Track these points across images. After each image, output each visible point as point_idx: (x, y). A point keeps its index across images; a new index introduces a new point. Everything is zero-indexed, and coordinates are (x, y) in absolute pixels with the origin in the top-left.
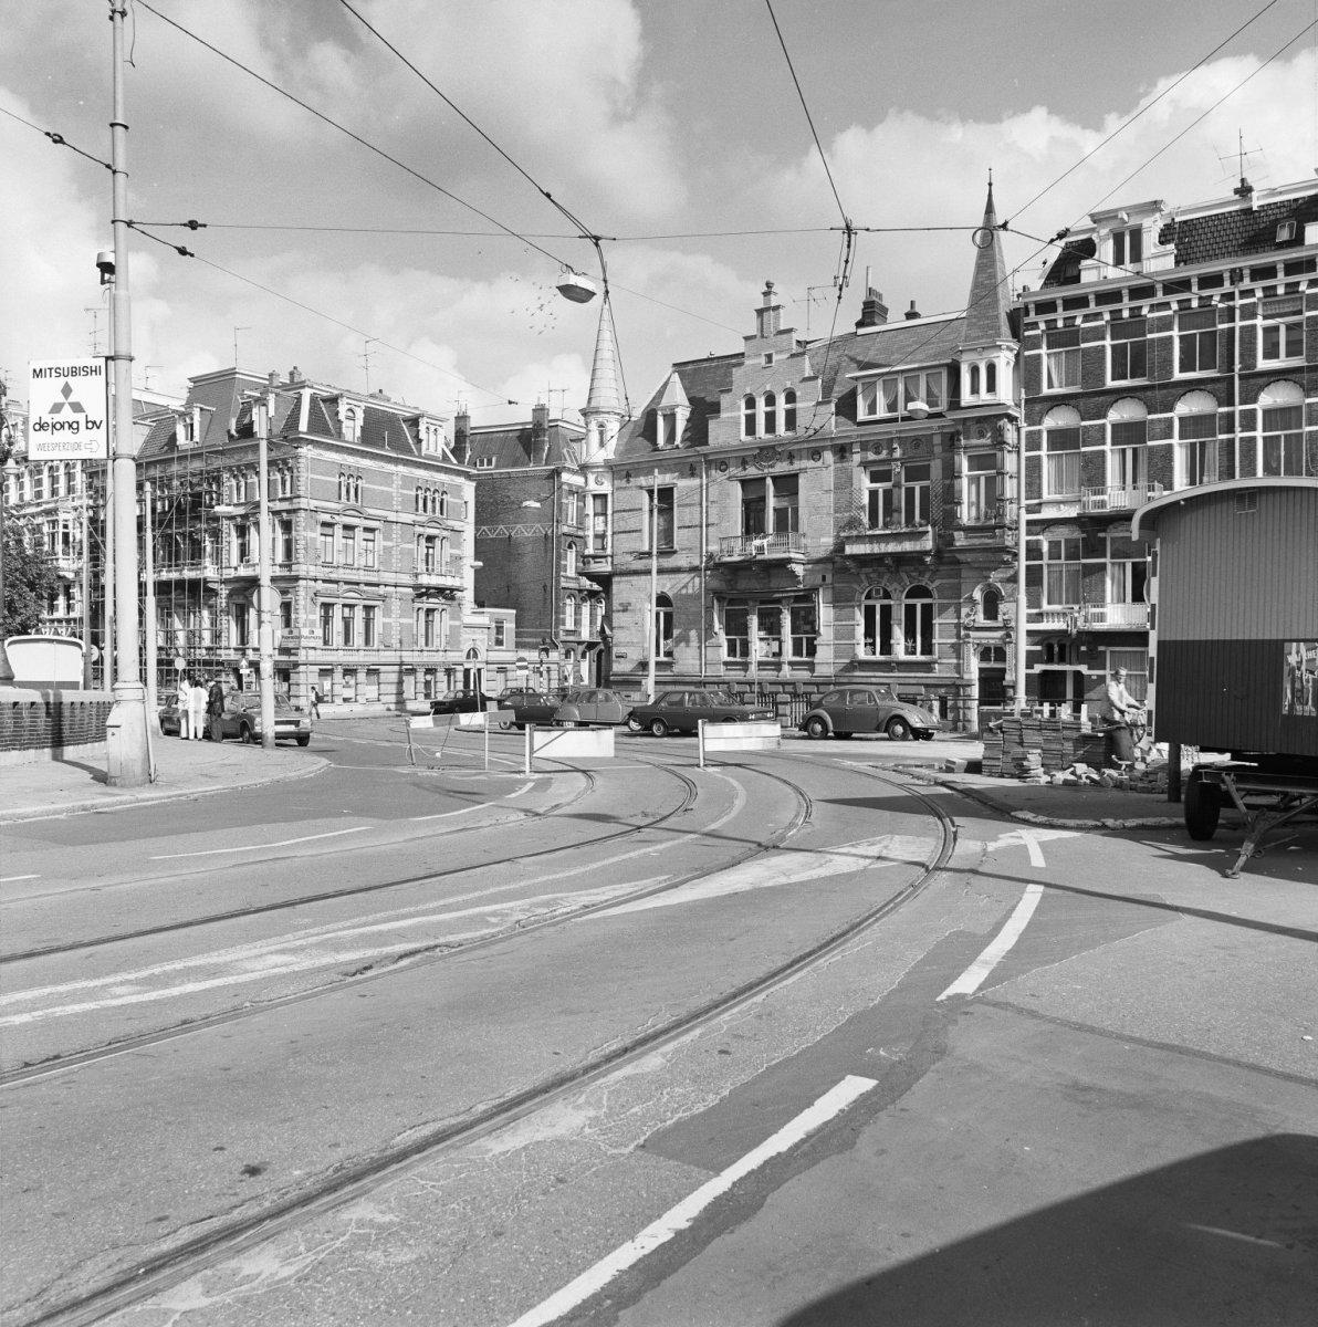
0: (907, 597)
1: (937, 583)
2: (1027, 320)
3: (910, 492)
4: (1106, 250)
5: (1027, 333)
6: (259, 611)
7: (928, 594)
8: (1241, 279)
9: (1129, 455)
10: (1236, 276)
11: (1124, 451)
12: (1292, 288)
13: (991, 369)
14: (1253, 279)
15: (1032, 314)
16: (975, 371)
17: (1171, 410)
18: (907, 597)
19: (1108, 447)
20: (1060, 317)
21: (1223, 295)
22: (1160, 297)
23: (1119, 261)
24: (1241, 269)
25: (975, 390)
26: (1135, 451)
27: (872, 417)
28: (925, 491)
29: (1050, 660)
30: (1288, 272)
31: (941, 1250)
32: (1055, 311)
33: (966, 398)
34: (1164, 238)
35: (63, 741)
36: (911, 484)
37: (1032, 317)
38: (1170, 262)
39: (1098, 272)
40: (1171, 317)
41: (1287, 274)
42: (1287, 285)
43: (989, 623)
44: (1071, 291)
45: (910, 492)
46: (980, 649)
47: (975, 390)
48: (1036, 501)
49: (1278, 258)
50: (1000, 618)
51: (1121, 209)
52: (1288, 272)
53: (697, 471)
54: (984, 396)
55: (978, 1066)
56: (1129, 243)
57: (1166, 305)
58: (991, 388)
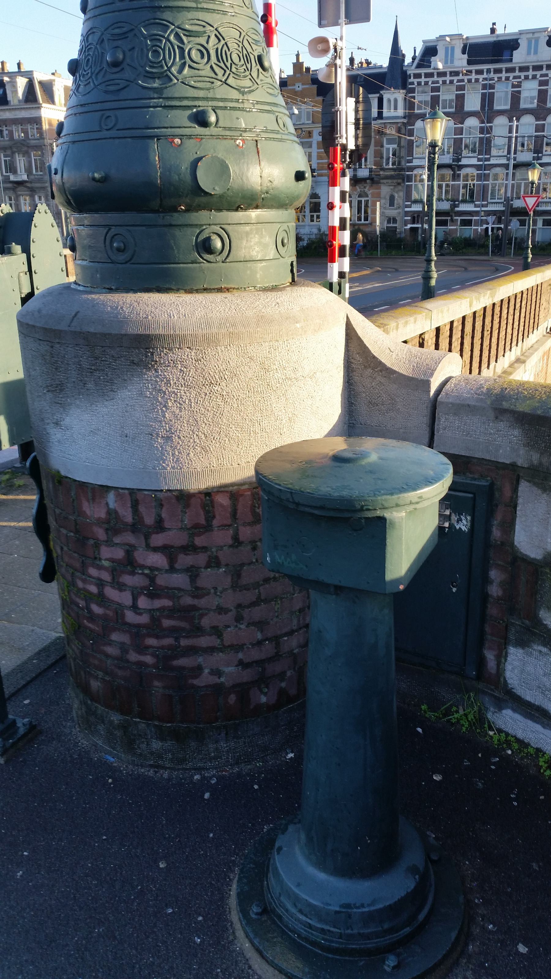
0: (358, 197)
1: (370, 192)
5: (410, 86)
6: (366, 160)
7: (367, 196)
8: (490, 73)
10: (489, 71)
12: (426, 83)
13: (396, 101)
14: (519, 71)
15: (412, 78)
16: (389, 101)
17: (545, 120)
18: (358, 197)
21: (483, 78)
23: (529, 53)
24: (490, 69)
29: (413, 223)
30: (451, 76)
31: (187, 495)
32: (421, 78)
38: (465, 62)
41: (533, 71)
44: (509, 65)
45: (388, 150)
46: (387, 218)
49: (503, 66)
51: (447, 35)
52: (451, 76)
54: (393, 113)
55: (348, 382)
58: (396, 108)
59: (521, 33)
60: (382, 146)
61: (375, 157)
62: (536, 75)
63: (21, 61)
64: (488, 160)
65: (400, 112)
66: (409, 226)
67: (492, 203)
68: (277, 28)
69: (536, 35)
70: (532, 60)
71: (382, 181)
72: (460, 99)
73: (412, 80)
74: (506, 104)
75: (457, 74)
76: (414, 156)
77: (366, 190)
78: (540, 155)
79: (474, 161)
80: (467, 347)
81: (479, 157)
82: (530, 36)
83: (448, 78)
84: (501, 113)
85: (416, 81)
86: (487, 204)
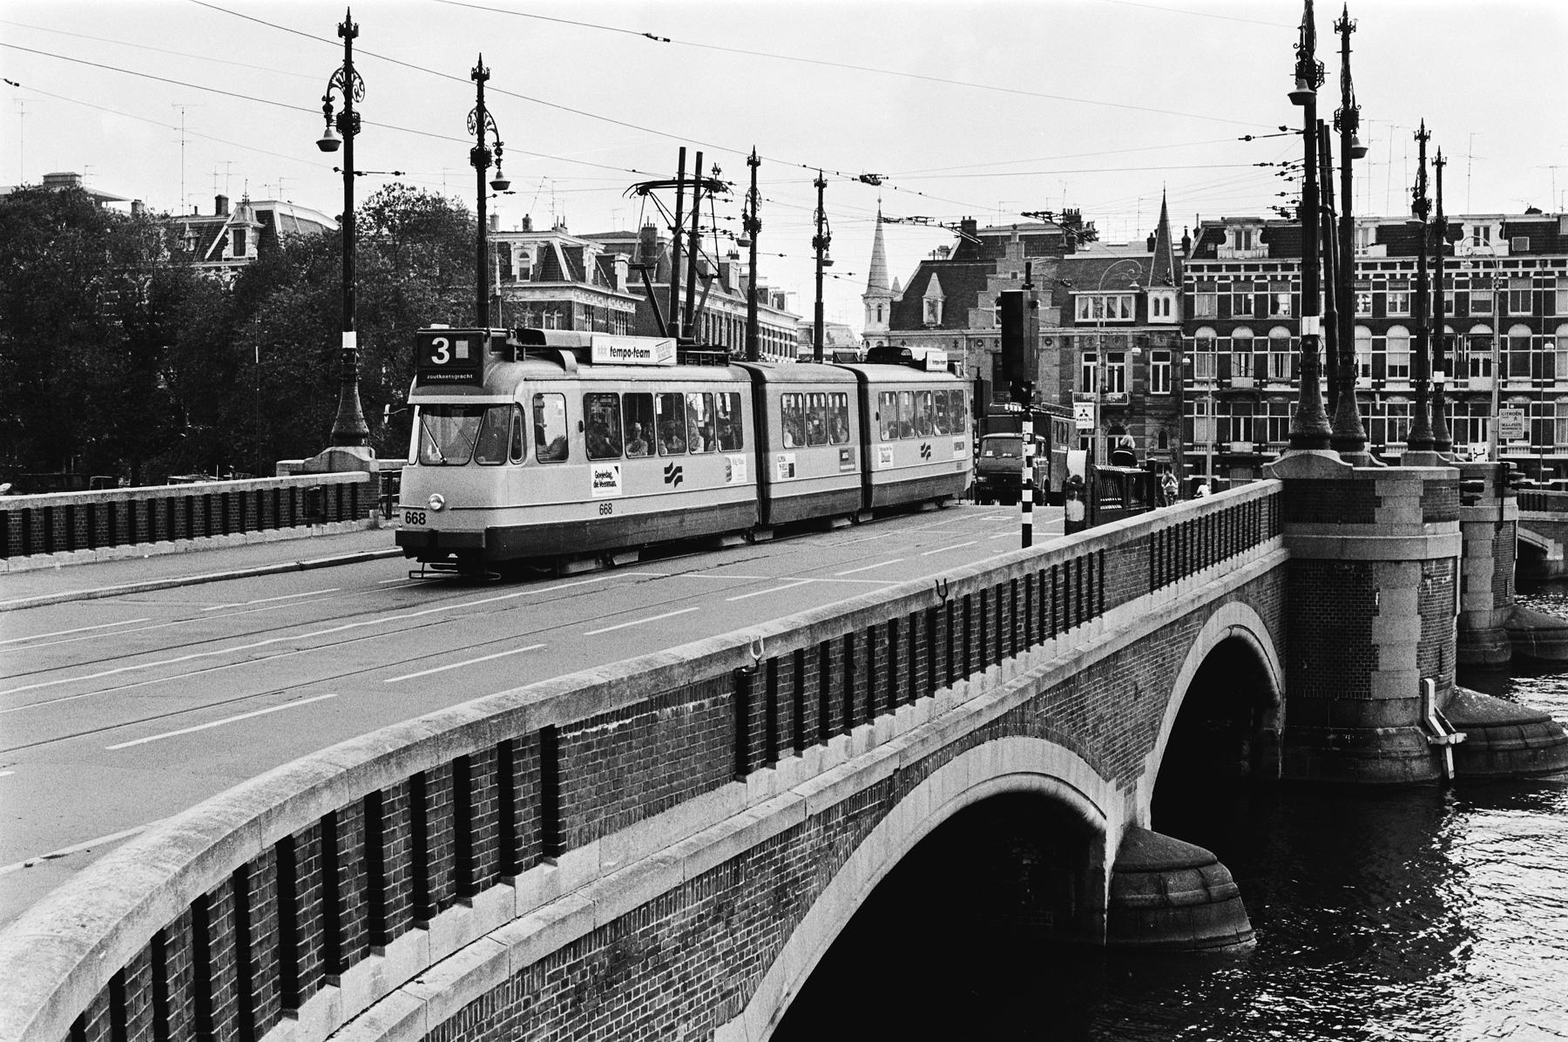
1: (1130, 425)
2: (1186, 274)
3: (1156, 368)
4: (1230, 239)
9: (1243, 357)
11: (1240, 355)
13: (1167, 302)
14: (1264, 270)
15: (1189, 271)
16: (1157, 301)
19: (1195, 352)
20: (1205, 274)
22: (1501, 269)
25: (1157, 313)
26: (1246, 356)
27: (1085, 320)
28: (1166, 368)
33: (1151, 318)
34: (1263, 240)
35: (155, 536)
36: (1157, 363)
37: (1189, 273)
39: (1226, 251)
40: (1193, 285)
42: (1524, 273)
43: (1162, 450)
44: (1213, 262)
45: (1156, 368)
47: (1157, 313)
48: (1552, 380)
50: (1169, 447)
53: (959, 345)
54: (1161, 319)
56: (1243, 241)
57: (1264, 277)
58: (1167, 313)
59: (1227, 222)
60: (1148, 363)
61: (1134, 378)
62: (1529, 273)
63: (530, 216)
64: (1552, 385)
65: (1173, 317)
66: (1191, 477)
67: (1391, 447)
68: (506, 214)
69: (1486, 223)
70: (1243, 255)
71: (1148, 412)
72: (1379, 301)
73: (1189, 273)
74: (1526, 309)
75: (1372, 266)
76: (1557, 377)
77: (1122, 424)
78: (1382, 381)
79: (1528, 388)
80: (122, 950)
81: (1535, 380)
82: (1238, 227)
83: (1242, 274)
84: (1361, 322)
85: (1195, 275)
86: (1193, 446)
